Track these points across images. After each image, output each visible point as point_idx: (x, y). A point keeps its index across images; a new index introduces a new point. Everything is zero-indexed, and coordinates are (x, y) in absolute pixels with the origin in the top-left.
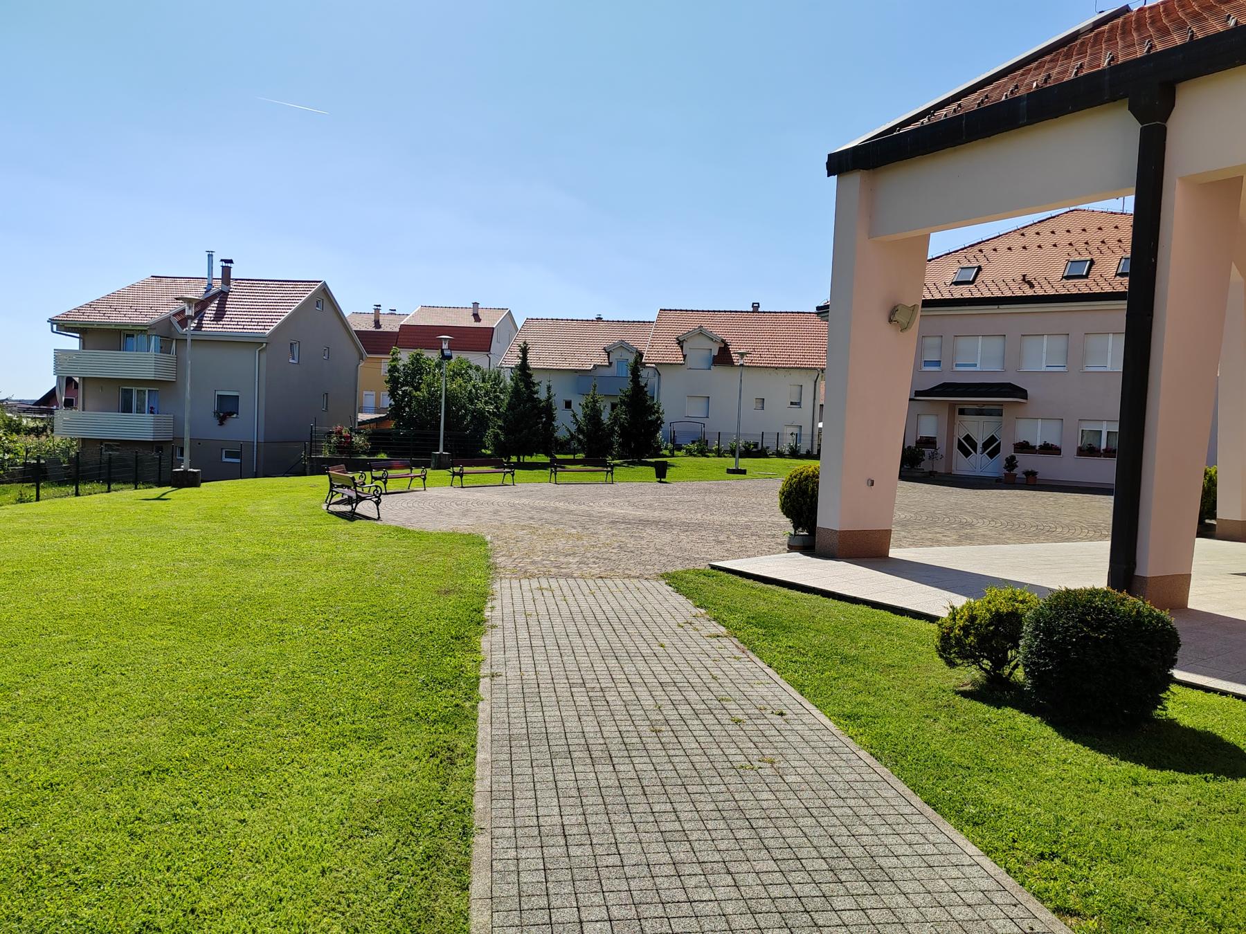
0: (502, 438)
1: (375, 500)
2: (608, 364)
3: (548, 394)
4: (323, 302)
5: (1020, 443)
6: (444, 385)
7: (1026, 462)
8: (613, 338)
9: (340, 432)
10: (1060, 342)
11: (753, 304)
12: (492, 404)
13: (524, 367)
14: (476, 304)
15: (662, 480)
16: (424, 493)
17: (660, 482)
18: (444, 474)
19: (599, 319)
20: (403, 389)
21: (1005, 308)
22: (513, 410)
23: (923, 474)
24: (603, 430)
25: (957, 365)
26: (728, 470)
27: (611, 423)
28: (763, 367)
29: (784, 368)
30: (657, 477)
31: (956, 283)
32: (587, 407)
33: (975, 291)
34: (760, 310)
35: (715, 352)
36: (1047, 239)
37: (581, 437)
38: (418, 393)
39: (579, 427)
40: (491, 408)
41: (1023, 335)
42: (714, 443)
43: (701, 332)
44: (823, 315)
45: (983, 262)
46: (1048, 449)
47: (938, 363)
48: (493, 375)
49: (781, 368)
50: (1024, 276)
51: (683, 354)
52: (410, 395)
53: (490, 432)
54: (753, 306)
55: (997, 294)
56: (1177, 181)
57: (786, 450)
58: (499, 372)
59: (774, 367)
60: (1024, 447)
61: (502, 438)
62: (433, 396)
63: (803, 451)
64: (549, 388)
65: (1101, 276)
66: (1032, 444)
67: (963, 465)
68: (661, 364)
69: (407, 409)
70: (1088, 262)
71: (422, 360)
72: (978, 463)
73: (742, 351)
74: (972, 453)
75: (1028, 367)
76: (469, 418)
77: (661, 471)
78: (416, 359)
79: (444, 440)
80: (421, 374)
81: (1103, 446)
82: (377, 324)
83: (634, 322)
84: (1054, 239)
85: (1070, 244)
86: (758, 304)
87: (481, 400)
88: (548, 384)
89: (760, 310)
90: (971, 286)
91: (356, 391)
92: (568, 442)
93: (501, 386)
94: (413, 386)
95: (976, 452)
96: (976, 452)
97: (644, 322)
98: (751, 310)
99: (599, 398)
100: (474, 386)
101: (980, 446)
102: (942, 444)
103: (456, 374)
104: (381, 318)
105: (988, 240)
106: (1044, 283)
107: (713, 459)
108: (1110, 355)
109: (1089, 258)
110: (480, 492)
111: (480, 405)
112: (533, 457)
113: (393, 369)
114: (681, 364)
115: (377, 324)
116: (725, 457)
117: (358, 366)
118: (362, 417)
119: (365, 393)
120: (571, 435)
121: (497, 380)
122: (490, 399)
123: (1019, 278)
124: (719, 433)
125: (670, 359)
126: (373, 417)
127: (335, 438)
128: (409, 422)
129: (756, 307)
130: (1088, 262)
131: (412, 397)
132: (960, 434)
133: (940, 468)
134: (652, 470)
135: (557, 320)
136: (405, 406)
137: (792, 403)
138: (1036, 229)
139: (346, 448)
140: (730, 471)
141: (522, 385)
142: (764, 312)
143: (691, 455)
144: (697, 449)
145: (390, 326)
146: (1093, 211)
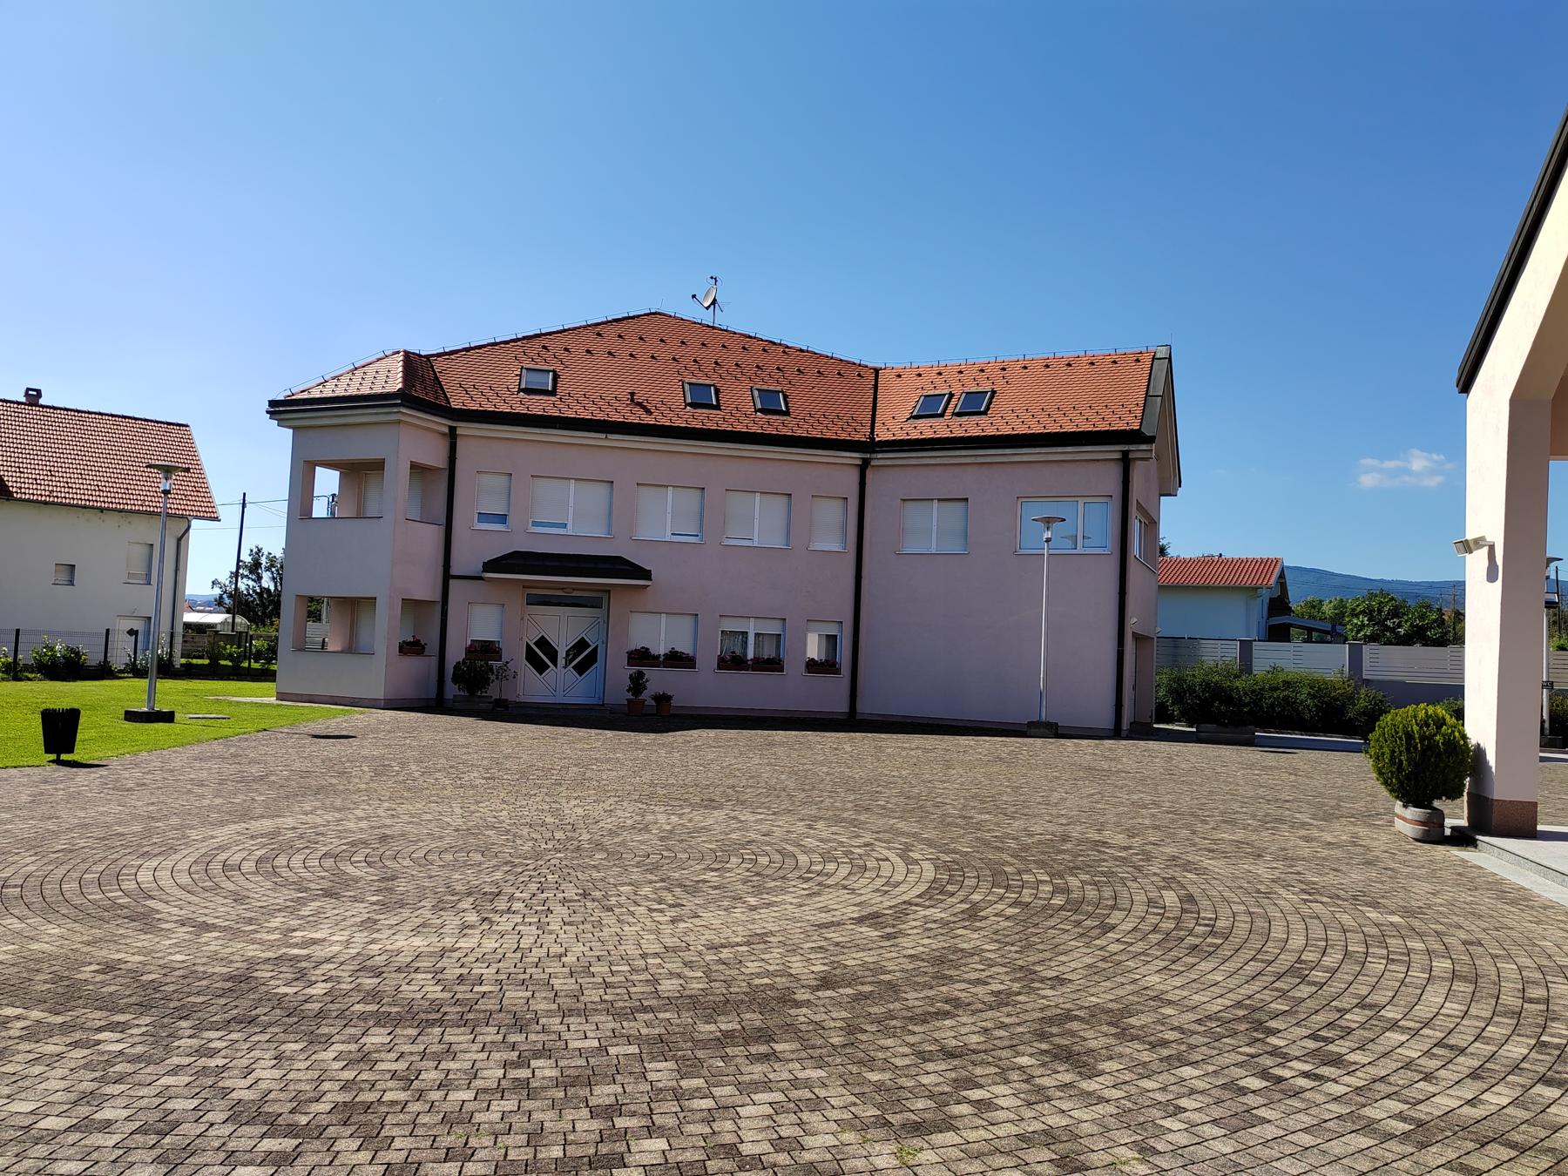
5: (636, 650)
11: (28, 389)
15: (64, 757)
17: (58, 762)
21: (616, 440)
25: (535, 524)
28: (77, 506)
29: (121, 511)
30: (47, 751)
34: (42, 401)
41: (727, 490)
44: (283, 416)
46: (677, 660)
47: (502, 519)
49: (112, 510)
54: (27, 395)
59: (97, 508)
60: (641, 657)
65: (505, 402)
66: (654, 651)
67: (532, 686)
70: (989, 393)
74: (549, 667)
75: (646, 533)
81: (750, 655)
90: (553, 399)
95: (556, 665)
96: (556, 665)
98: (23, 400)
101: (561, 655)
109: (947, 391)
116: (29, 679)
123: (626, 397)
124: (18, 631)
129: (33, 397)
130: (989, 393)
138: (620, 329)
140: (131, 716)
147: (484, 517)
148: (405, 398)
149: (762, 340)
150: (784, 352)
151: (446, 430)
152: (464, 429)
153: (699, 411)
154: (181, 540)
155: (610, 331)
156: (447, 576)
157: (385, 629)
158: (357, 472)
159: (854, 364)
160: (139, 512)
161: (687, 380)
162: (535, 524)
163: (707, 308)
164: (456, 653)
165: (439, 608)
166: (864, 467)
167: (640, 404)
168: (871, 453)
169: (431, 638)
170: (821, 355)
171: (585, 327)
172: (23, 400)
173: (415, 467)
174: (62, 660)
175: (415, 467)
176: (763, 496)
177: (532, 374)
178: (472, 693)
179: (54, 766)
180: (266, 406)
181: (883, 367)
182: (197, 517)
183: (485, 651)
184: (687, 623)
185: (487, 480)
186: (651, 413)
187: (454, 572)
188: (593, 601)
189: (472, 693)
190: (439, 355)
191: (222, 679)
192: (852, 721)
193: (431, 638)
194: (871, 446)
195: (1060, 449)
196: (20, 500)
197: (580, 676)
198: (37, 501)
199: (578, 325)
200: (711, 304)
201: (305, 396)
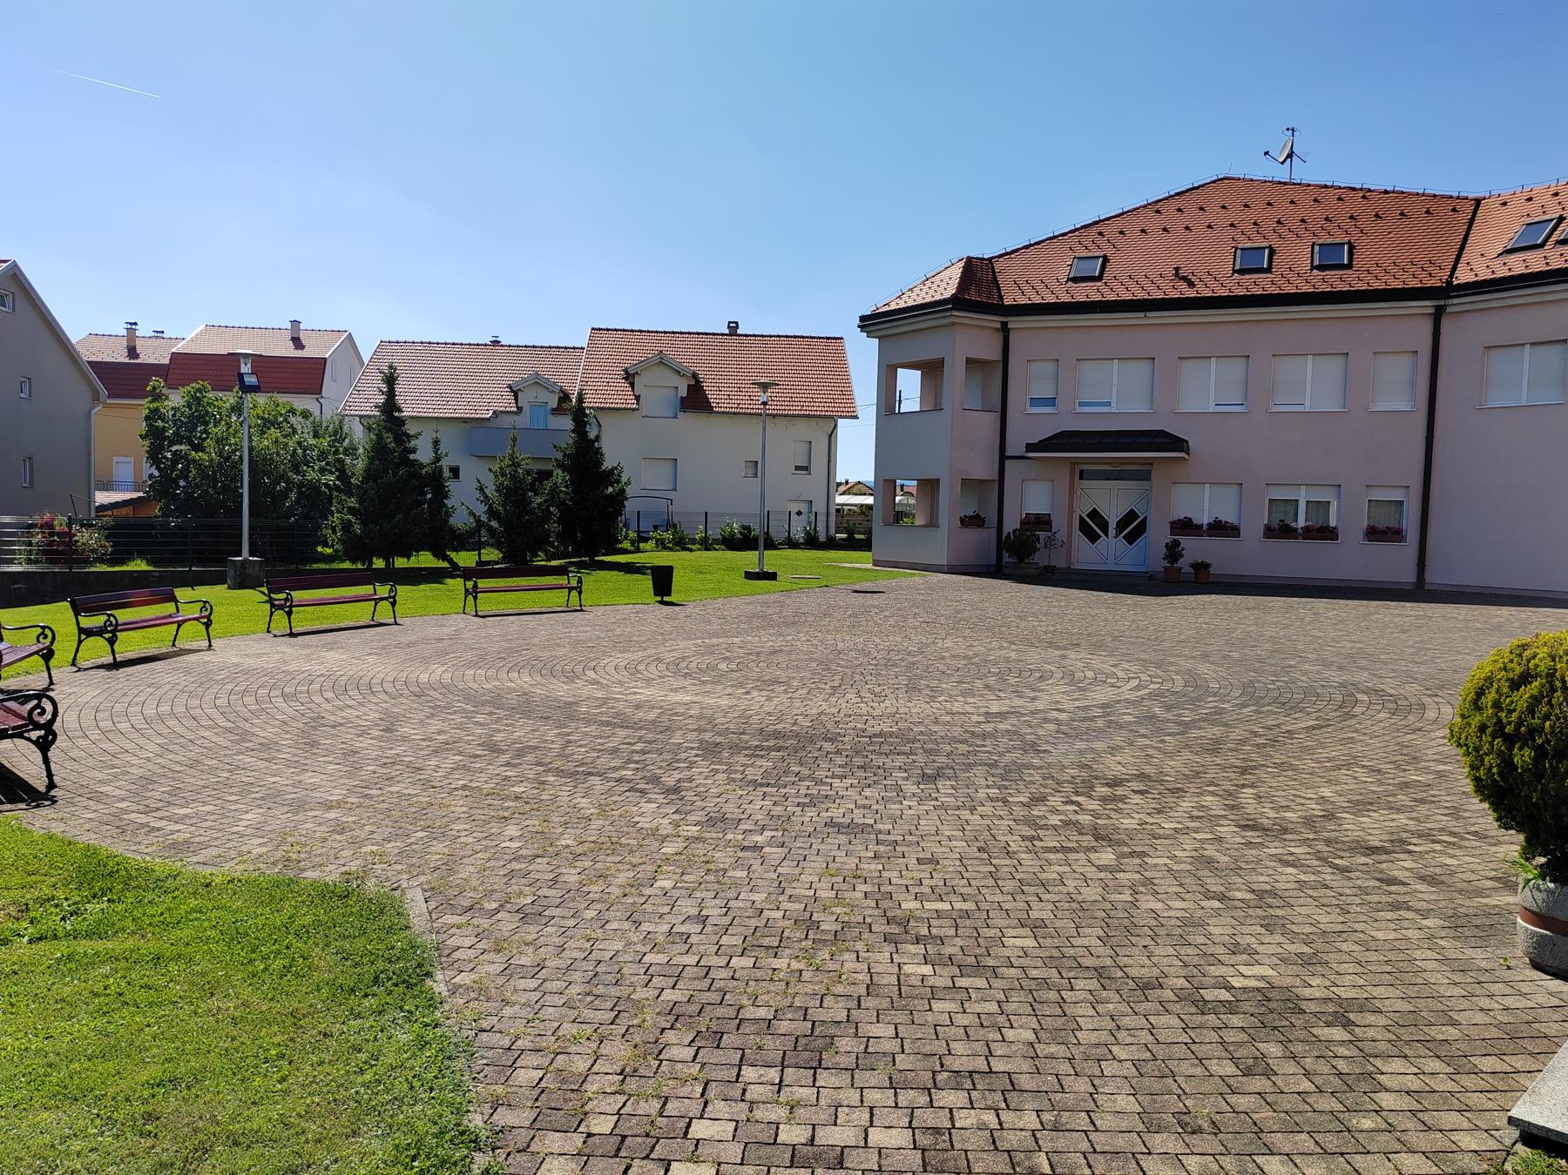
0: (357, 528)
1: (34, 735)
2: (515, 409)
3: (436, 453)
4: (14, 299)
6: (245, 441)
7: (1194, 548)
8: (520, 372)
9: (50, 525)
10: (1237, 366)
11: (730, 323)
12: (332, 473)
13: (390, 405)
14: (295, 323)
15: (666, 599)
16: (206, 656)
17: (662, 602)
18: (253, 599)
19: (496, 343)
20: (174, 448)
21: (1155, 317)
22: (375, 481)
23: (1037, 572)
24: (532, 511)
25: (1081, 404)
26: (746, 572)
27: (546, 501)
29: (786, 416)
30: (656, 594)
31: (1075, 280)
32: (503, 474)
33: (1105, 290)
34: (739, 332)
35: (683, 392)
36: (1214, 215)
37: (494, 524)
38: (200, 454)
39: (491, 507)
40: (331, 479)
41: (1180, 358)
42: (697, 529)
43: (662, 361)
44: (872, 328)
45: (1109, 252)
46: (1221, 529)
47: (1051, 402)
48: (331, 426)
50: (1177, 269)
51: (634, 395)
52: (186, 459)
53: (336, 519)
54: (729, 327)
55: (1141, 295)
56: (574, 400)
57: (799, 536)
58: (341, 422)
60: (1185, 526)
61: (357, 528)
62: (228, 459)
63: (822, 538)
64: (436, 443)
66: (1196, 521)
67: (1087, 555)
68: (602, 409)
69: (182, 483)
71: (206, 400)
72: (1111, 552)
73: (763, 380)
76: (293, 496)
77: (662, 581)
78: (196, 400)
79: (250, 536)
80: (206, 423)
82: (132, 352)
83: (550, 347)
84: (1206, 218)
85: (1232, 225)
86: (736, 323)
87: (312, 467)
88: (434, 435)
89: (739, 332)
90: (1099, 284)
91: (89, 454)
92: (471, 533)
93: (345, 445)
94: (190, 443)
97: (566, 348)
98: (727, 331)
99: (523, 459)
100: (299, 443)
102: (1059, 523)
103: (268, 423)
104: (138, 343)
105: (1108, 219)
106: (1208, 279)
107: (698, 552)
108: (1308, 386)
110: (331, 647)
111: (311, 475)
112: (413, 558)
113: (154, 415)
114: (633, 410)
115: (132, 352)
116: (716, 550)
117: (90, 412)
118: (102, 498)
119: (115, 459)
120: (478, 521)
121: (338, 434)
122: (327, 464)
125: (615, 401)
126: (128, 498)
127: (40, 536)
128: (187, 505)
129: (733, 328)
130: (1267, 251)
131: (189, 462)
132: (1083, 509)
133: (1060, 562)
134: (647, 582)
135: (430, 343)
136: (179, 477)
137: (797, 468)
139: (61, 553)
141: (389, 438)
142: (747, 336)
143: (665, 548)
144: (673, 539)
145: (152, 355)
146: (1252, 180)
147: (1035, 402)
148: (958, 302)
149: (1340, 188)
150: (1364, 197)
151: (999, 326)
152: (1014, 323)
153: (1247, 276)
154: (831, 436)
155: (1190, 203)
156: (1003, 457)
157: (951, 504)
158: (932, 370)
159: (1451, 197)
160: (799, 416)
161: (1240, 246)
162: (1081, 404)
163: (1282, 163)
164: (1011, 524)
165: (996, 486)
166: (1438, 315)
167: (1185, 279)
168: (1445, 299)
169: (991, 516)
170: (1409, 194)
171: (1145, 206)
172: (727, 331)
173: (970, 362)
174: (739, 536)
175: (970, 362)
176: (1317, 358)
177: (1082, 262)
178: (1021, 560)
179: (658, 604)
180: (857, 321)
181: (1487, 195)
182: (841, 417)
183: (1041, 522)
184: (1232, 492)
185: (1038, 368)
186: (1194, 286)
187: (1008, 454)
188: (1142, 474)
189: (1021, 560)
190: (1001, 256)
191: (860, 550)
192: (1420, 591)
193: (991, 516)
194: (1450, 290)
195: (1086, 316)
196: (718, 412)
197: (1131, 544)
198: (729, 413)
199: (1138, 205)
200: (1287, 157)
201: (886, 309)
